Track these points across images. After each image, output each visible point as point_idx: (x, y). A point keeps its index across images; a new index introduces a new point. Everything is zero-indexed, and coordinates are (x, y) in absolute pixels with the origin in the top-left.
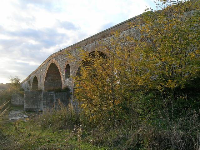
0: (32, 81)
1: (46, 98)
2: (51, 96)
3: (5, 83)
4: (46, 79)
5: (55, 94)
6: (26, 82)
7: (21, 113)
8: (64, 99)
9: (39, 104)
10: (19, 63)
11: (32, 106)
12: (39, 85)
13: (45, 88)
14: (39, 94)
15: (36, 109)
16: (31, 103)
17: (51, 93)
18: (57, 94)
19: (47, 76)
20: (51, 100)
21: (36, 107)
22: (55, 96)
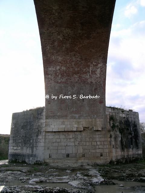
11: (22, 149)
15: (29, 156)
16: (20, 141)
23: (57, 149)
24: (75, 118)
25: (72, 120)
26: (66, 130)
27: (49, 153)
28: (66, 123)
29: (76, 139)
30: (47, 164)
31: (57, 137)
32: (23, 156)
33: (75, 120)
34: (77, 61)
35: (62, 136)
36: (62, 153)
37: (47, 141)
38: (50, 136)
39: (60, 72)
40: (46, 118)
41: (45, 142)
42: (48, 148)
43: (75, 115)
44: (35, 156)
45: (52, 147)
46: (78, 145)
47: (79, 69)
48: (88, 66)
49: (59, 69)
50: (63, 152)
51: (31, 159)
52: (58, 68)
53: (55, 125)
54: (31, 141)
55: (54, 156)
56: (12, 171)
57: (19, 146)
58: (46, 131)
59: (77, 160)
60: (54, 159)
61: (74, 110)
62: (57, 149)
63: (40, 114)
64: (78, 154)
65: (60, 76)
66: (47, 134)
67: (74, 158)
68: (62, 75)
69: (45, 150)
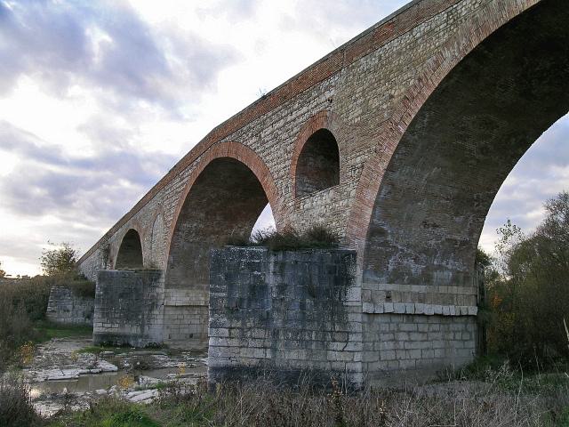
0: (118, 248)
1: (228, 277)
2: (252, 267)
3: (32, 275)
4: (177, 229)
5: (272, 259)
6: (98, 251)
7: (81, 352)
8: (315, 282)
9: (149, 319)
10: (80, 231)
11: (122, 326)
12: (145, 254)
14: (149, 282)
15: (135, 337)
17: (253, 255)
18: (280, 257)
19: (184, 217)
20: (253, 288)
21: (135, 330)
22: (271, 267)
24: (202, 289)
25: (198, 291)
28: (191, 295)
29: (202, 315)
30: (166, 347)
31: (179, 312)
32: (125, 336)
35: (185, 312)
37: (167, 317)
38: (171, 312)
40: (167, 286)
42: (168, 328)
44: (147, 337)
48: (232, 228)
50: (186, 331)
51: (140, 340)
53: (178, 297)
55: (175, 337)
56: (441, 316)
60: (174, 340)
63: (156, 280)
66: (167, 309)
68: (197, 234)
69: (163, 328)
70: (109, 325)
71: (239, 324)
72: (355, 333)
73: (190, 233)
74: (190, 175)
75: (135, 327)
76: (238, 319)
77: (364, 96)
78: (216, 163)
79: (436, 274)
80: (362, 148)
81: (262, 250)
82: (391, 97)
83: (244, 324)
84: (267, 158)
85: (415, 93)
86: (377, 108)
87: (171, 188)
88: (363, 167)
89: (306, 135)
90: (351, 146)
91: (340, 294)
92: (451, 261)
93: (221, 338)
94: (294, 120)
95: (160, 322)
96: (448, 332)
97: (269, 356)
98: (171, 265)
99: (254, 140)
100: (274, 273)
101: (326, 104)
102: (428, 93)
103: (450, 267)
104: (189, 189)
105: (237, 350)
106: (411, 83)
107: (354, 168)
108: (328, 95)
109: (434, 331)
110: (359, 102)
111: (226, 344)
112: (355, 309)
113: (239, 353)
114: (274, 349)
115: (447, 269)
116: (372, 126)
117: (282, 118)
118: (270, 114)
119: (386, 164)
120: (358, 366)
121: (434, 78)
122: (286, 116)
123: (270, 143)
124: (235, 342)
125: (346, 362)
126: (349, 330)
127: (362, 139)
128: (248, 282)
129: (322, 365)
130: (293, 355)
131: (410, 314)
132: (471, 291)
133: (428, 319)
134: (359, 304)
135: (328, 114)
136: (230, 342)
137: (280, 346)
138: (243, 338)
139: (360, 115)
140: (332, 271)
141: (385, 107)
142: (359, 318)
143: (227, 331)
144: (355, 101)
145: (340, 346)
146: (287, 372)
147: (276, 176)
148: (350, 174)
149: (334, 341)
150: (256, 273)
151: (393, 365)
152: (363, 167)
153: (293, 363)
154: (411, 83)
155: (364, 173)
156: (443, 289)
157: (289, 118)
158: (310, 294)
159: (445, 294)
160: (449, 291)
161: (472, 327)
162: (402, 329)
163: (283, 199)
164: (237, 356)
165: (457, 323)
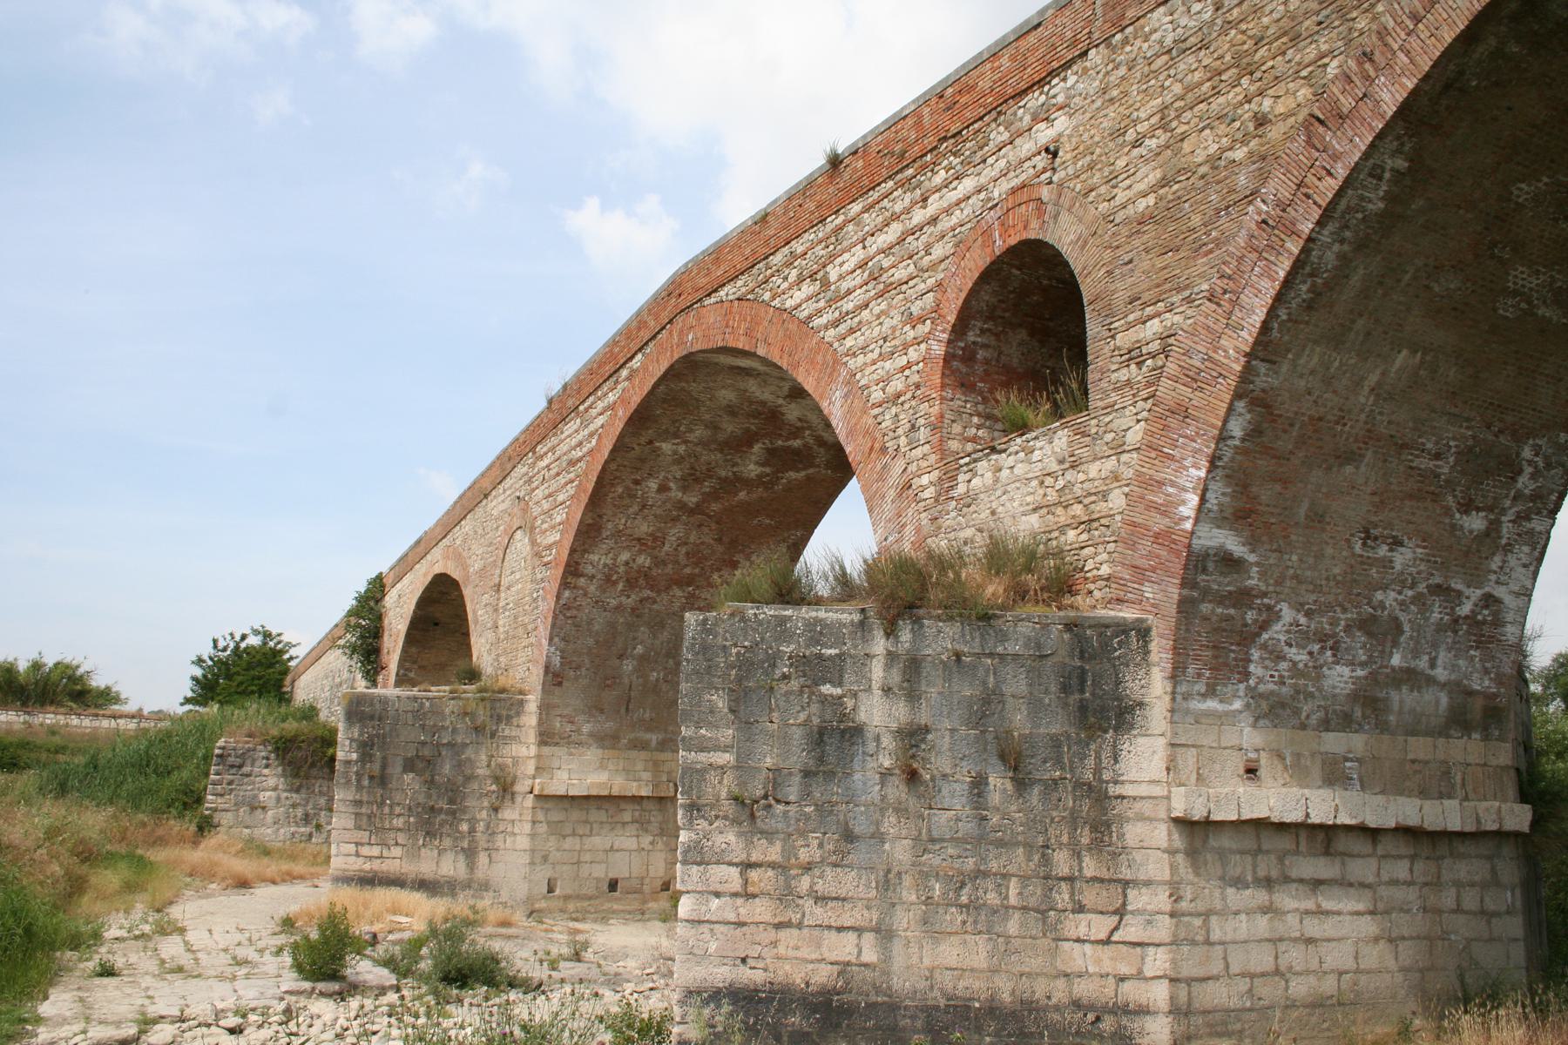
4: (572, 570)
9: (491, 833)
13: (557, 660)
17: (818, 634)
19: (587, 533)
22: (877, 671)
23: (578, 862)
24: (642, 746)
25: (634, 754)
26: (615, 792)
27: (548, 875)
33: (644, 755)
34: (702, 543)
36: (595, 875)
39: (627, 572)
41: (533, 836)
42: (545, 859)
43: (648, 736)
45: (558, 854)
46: (651, 847)
47: (697, 571)
49: (627, 563)
50: (599, 871)
52: (625, 556)
54: (464, 827)
57: (397, 844)
58: (545, 793)
59: (645, 902)
61: (647, 715)
62: (578, 862)
63: (509, 718)
64: (647, 881)
65: (620, 586)
67: (636, 895)
68: (631, 584)
69: (532, 863)
70: (376, 851)
71: (774, 852)
72: (1148, 883)
73: (609, 581)
74: (612, 407)
75: (450, 856)
76: (769, 835)
77: (1165, 127)
78: (689, 366)
79: (1402, 699)
80: (1164, 290)
81: (845, 618)
82: (1261, 121)
83: (789, 852)
84: (849, 342)
85: (1347, 103)
86: (1213, 161)
87: (553, 449)
88: (1165, 351)
89: (977, 261)
90: (1121, 291)
91: (1098, 757)
92: (1443, 657)
93: (717, 895)
94: (934, 221)
95: (523, 842)
96: (1436, 884)
97: (870, 956)
98: (554, 678)
99: (808, 289)
100: (887, 690)
101: (1041, 161)
102: (1390, 97)
103: (1441, 673)
104: (619, 425)
105: (772, 934)
106: (1333, 68)
107: (1134, 356)
108: (1044, 134)
109: (1394, 882)
110: (907, 406)
111: (732, 917)
112: (1146, 807)
113: (774, 944)
114: (884, 933)
115: (1431, 681)
116: (1196, 220)
117: (896, 217)
118: (856, 208)
119: (1247, 337)
120: (1159, 994)
121: (1414, 43)
122: (908, 211)
123: (858, 297)
124: (761, 910)
125: (1122, 979)
126: (1126, 874)
127: (1159, 263)
128: (802, 717)
129: (1040, 989)
130: (950, 953)
131: (1321, 826)
132: (1504, 755)
133: (1375, 842)
134: (1158, 791)
135: (1045, 193)
136: (745, 910)
137: (904, 920)
138: (786, 896)
139: (1153, 189)
140: (1072, 682)
141: (1239, 154)
142: (1161, 834)
143: (734, 872)
144: (1137, 144)
145: (1099, 926)
146: (930, 1011)
147: (877, 395)
148: (1123, 375)
149: (1080, 909)
150: (827, 689)
151: (1269, 991)
152: (1165, 351)
153: (946, 980)
154: (1333, 68)
155: (1171, 367)
156: (1420, 747)
157: (919, 216)
158: (1002, 757)
159: (1427, 762)
160: (1441, 756)
161: (1509, 870)
162: (1294, 874)
163: (899, 465)
164: (768, 953)
165: (1462, 856)
